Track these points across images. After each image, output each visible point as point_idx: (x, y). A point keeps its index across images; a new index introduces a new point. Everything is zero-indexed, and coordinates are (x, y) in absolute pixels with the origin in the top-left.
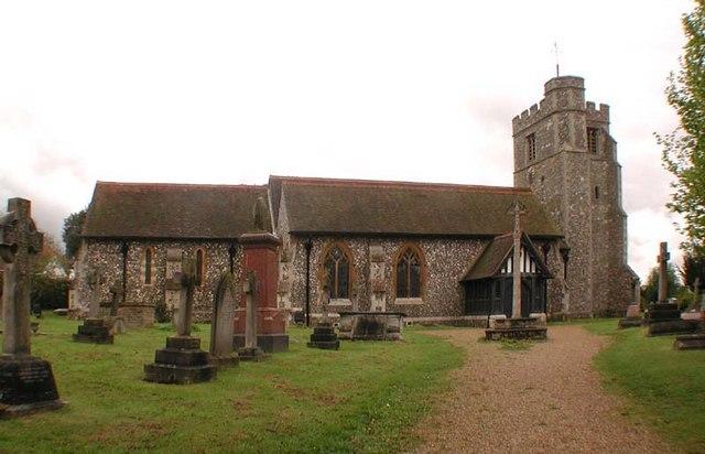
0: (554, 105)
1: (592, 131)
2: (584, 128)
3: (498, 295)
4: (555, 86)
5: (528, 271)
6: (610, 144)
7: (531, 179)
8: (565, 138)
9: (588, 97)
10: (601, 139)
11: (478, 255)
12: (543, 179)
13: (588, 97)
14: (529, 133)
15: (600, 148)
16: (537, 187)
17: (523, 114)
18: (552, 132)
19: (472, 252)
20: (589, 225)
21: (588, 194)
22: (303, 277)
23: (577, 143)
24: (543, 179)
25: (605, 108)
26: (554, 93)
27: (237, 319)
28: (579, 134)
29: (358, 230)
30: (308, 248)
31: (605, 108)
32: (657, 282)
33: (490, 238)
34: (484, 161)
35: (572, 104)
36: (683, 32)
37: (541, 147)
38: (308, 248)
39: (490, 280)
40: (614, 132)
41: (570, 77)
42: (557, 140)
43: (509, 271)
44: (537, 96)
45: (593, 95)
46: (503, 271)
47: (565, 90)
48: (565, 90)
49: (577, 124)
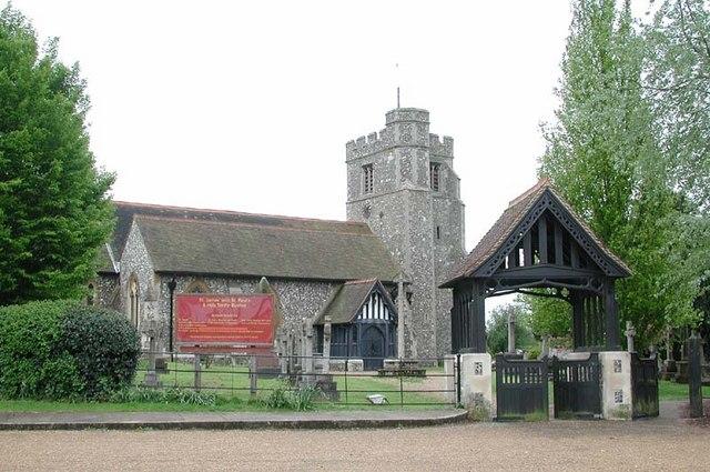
0: (397, 139)
1: (435, 166)
2: (427, 165)
3: (355, 339)
4: (396, 118)
5: (376, 316)
6: (453, 181)
7: (367, 211)
8: (406, 175)
9: (433, 129)
10: (444, 174)
11: (329, 299)
12: (381, 215)
13: (433, 129)
14: (364, 162)
15: (442, 188)
16: (373, 222)
17: (370, 137)
18: (393, 165)
19: (325, 296)
20: (432, 269)
21: (431, 236)
22: (167, 317)
23: (419, 182)
24: (381, 215)
25: (449, 141)
26: (397, 126)
27: (617, 372)
28: (421, 167)
29: (218, 271)
30: (172, 287)
31: (449, 141)
32: (390, 332)
33: (342, 282)
34: (318, 194)
35: (415, 139)
36: (559, 59)
37: (380, 180)
38: (172, 287)
39: (347, 325)
40: (458, 166)
41: (414, 110)
42: (399, 177)
43: (365, 317)
44: (379, 124)
45: (438, 127)
46: (360, 317)
47: (409, 121)
48: (409, 121)
49: (419, 161)
